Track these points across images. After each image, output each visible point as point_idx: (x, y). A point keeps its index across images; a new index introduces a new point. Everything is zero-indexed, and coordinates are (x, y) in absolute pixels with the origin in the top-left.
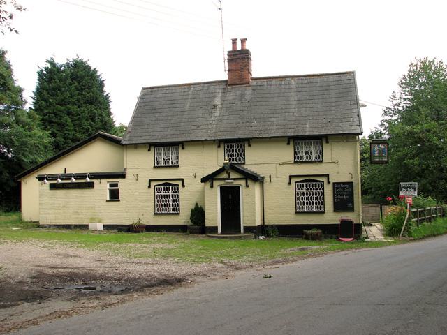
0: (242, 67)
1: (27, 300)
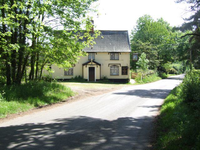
1: (70, 79)
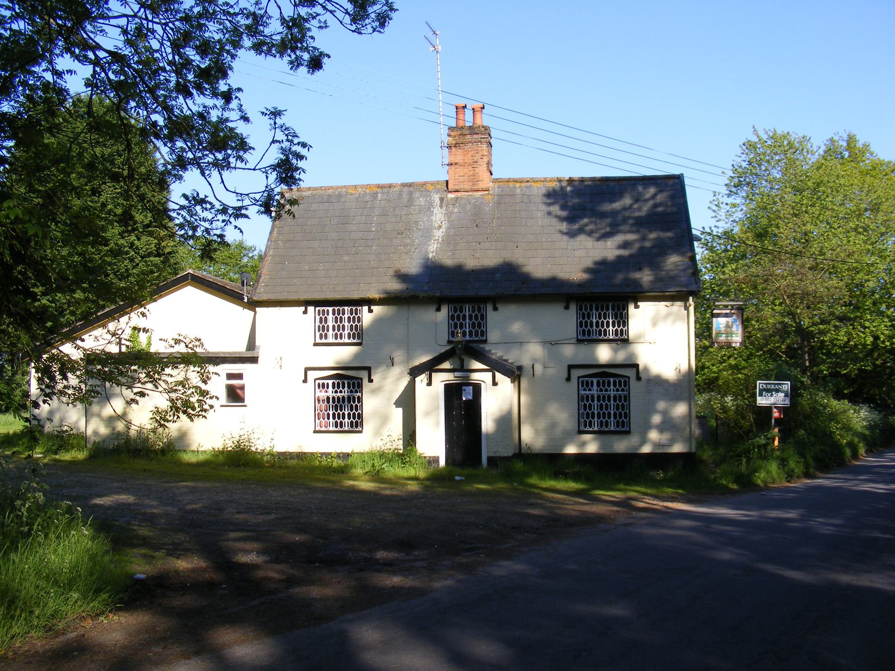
0: (476, 159)
